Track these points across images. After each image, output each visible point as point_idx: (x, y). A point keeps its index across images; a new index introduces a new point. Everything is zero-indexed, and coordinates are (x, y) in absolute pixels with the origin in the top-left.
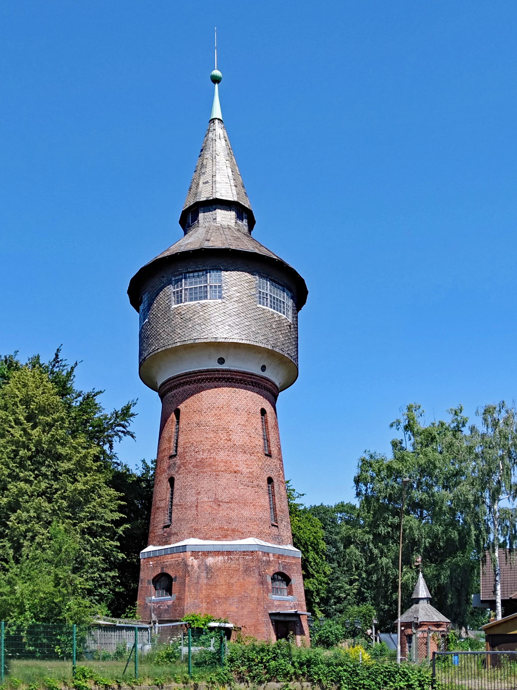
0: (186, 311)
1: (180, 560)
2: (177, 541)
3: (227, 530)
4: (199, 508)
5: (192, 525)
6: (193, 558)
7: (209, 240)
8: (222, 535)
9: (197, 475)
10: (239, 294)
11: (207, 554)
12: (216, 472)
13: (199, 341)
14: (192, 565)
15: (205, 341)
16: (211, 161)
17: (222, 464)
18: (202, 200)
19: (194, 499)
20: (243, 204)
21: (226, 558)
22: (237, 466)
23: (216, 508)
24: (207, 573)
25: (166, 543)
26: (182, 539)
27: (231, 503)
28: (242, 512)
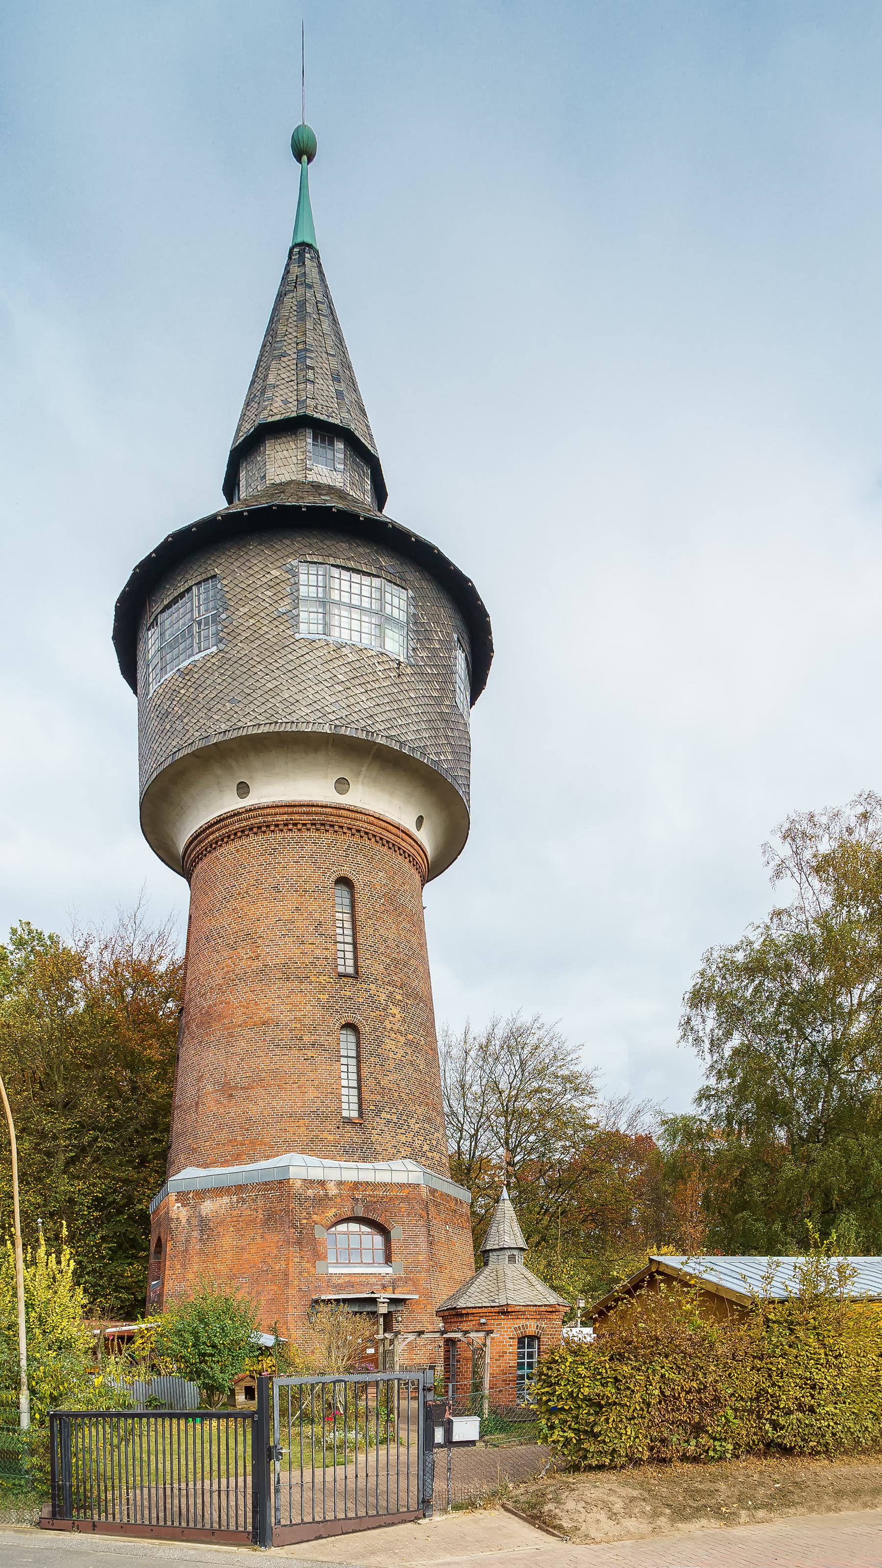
3: (242, 1144)
6: (179, 1205)
10: (252, 621)
14: (178, 1219)
21: (235, 1198)
28: (274, 1103)
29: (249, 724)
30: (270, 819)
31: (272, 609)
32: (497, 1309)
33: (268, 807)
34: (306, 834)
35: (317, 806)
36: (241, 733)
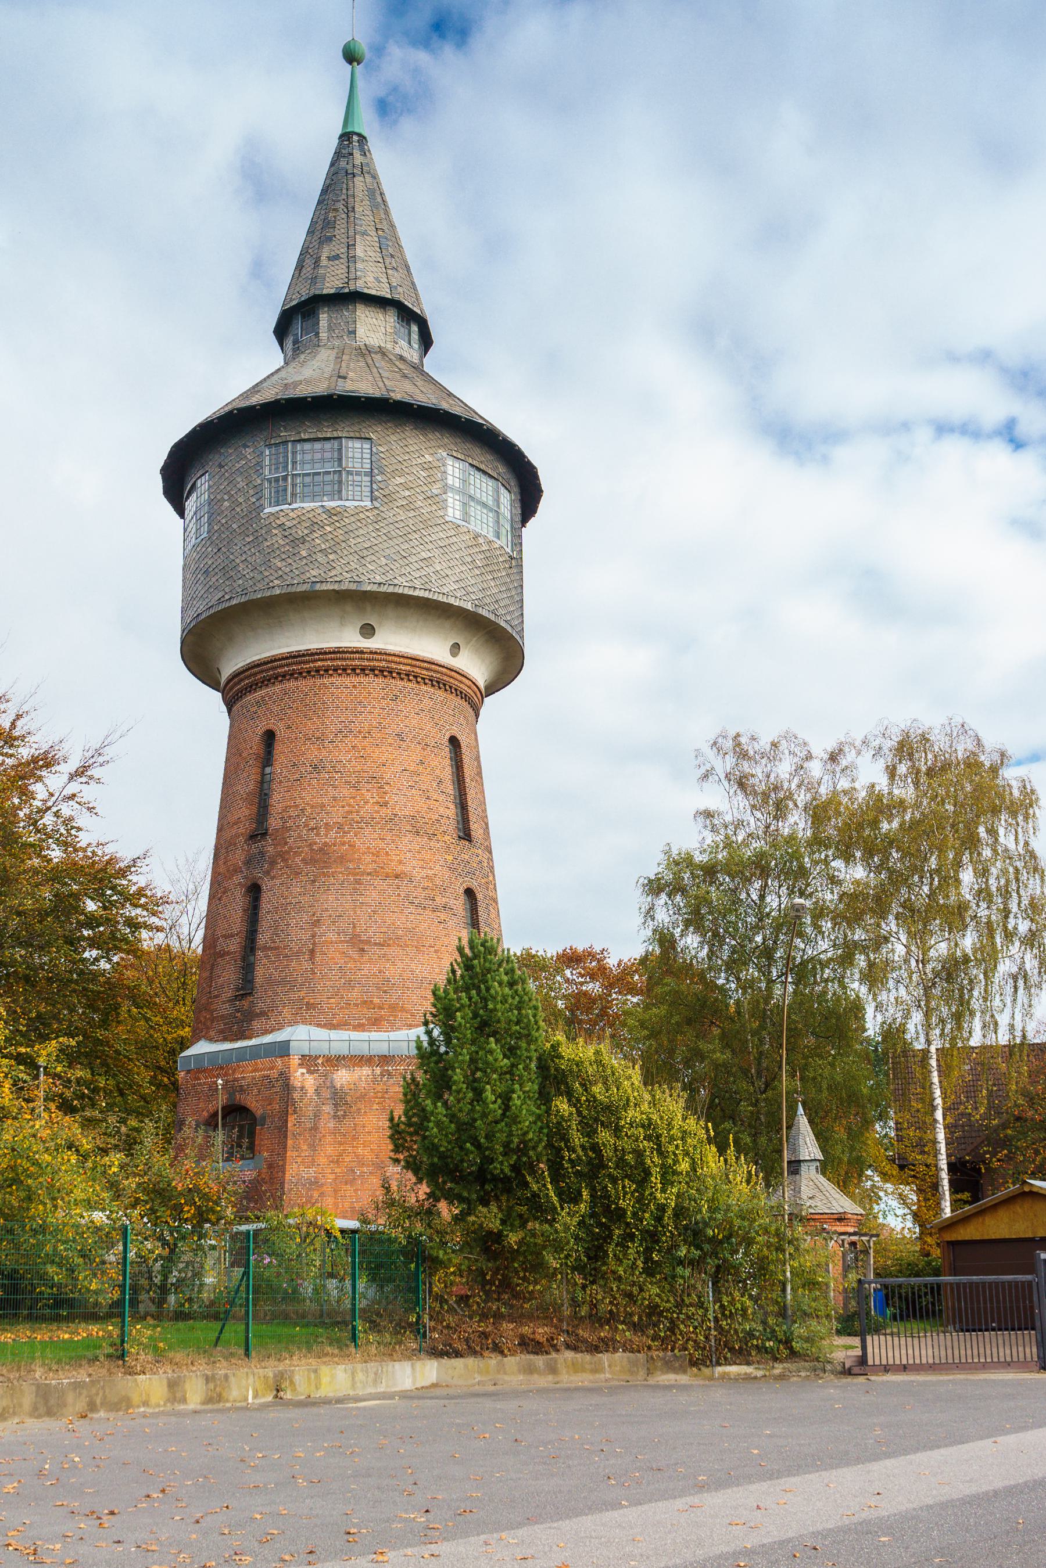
0: (295, 522)
1: (274, 1074)
2: (266, 1032)
3: (381, 1008)
4: (318, 958)
5: (302, 994)
6: (304, 1071)
7: (345, 378)
8: (369, 1019)
9: (314, 881)
10: (407, 493)
11: (335, 1061)
12: (354, 875)
13: (324, 587)
14: (302, 1088)
15: (336, 587)
16: (344, 216)
17: (368, 858)
18: (325, 292)
19: (305, 936)
20: (410, 306)
21: (378, 1070)
22: (400, 862)
23: (356, 956)
24: (336, 1105)
25: (242, 1036)
26: (280, 1027)
27: (389, 945)
28: (413, 966)
29: (405, 584)
30: (394, 666)
31: (426, 488)
32: (836, 1216)
33: (394, 655)
34: (424, 688)
35: (437, 665)
36: (397, 590)
